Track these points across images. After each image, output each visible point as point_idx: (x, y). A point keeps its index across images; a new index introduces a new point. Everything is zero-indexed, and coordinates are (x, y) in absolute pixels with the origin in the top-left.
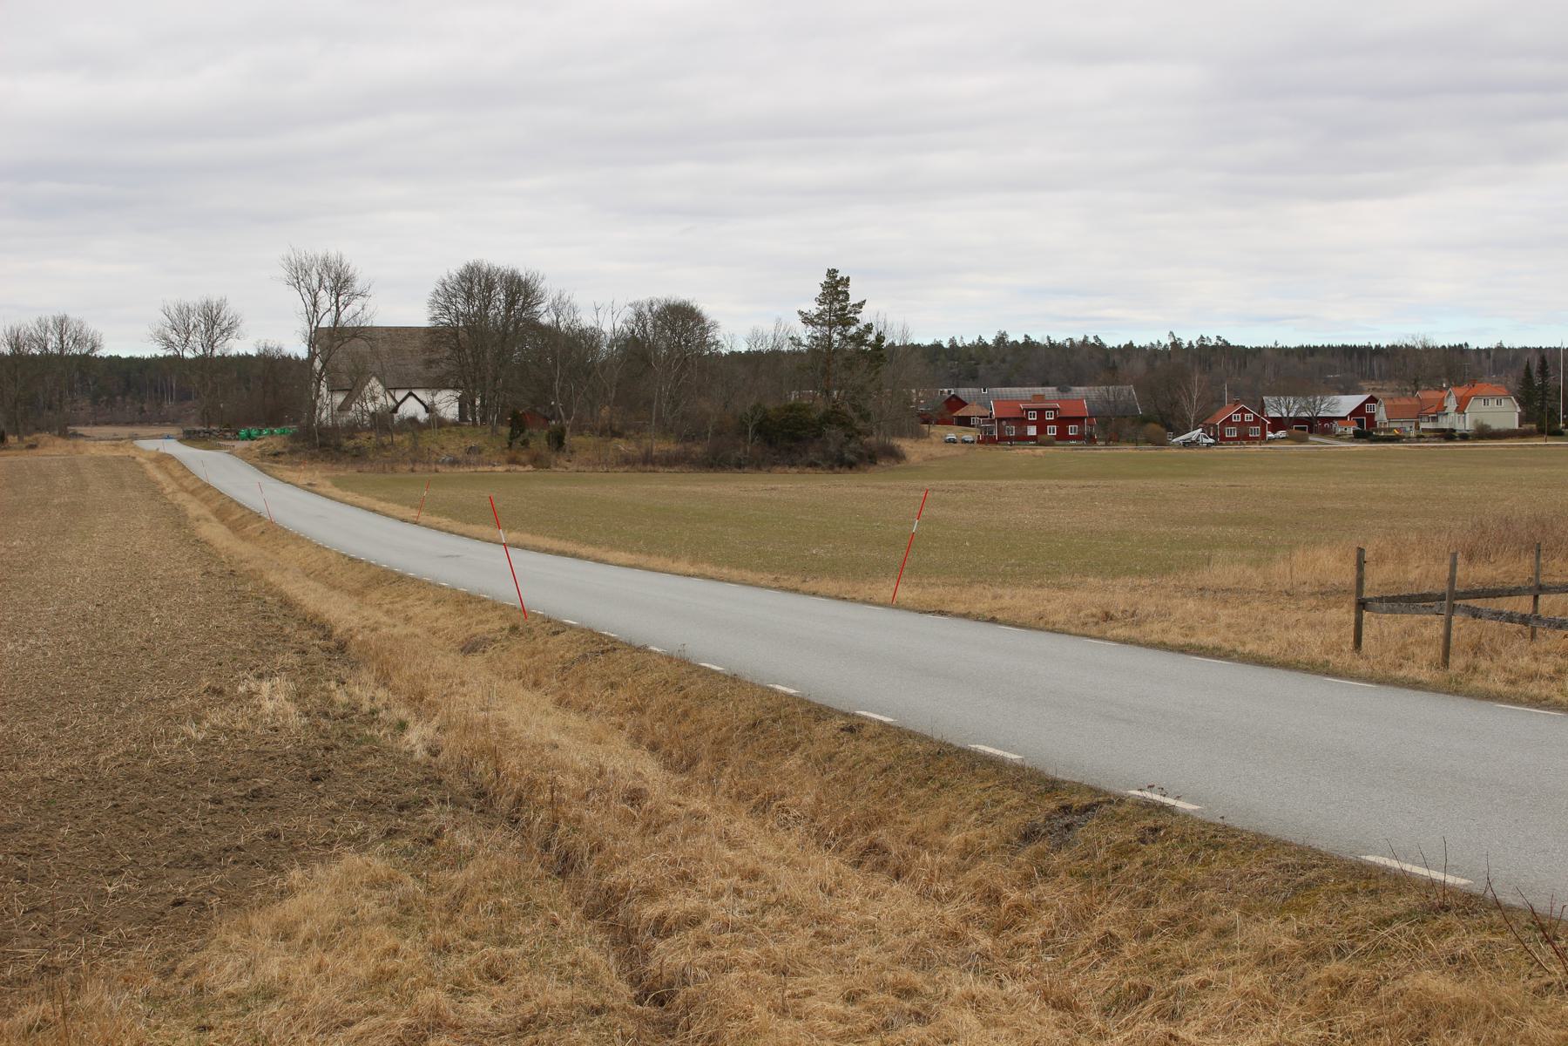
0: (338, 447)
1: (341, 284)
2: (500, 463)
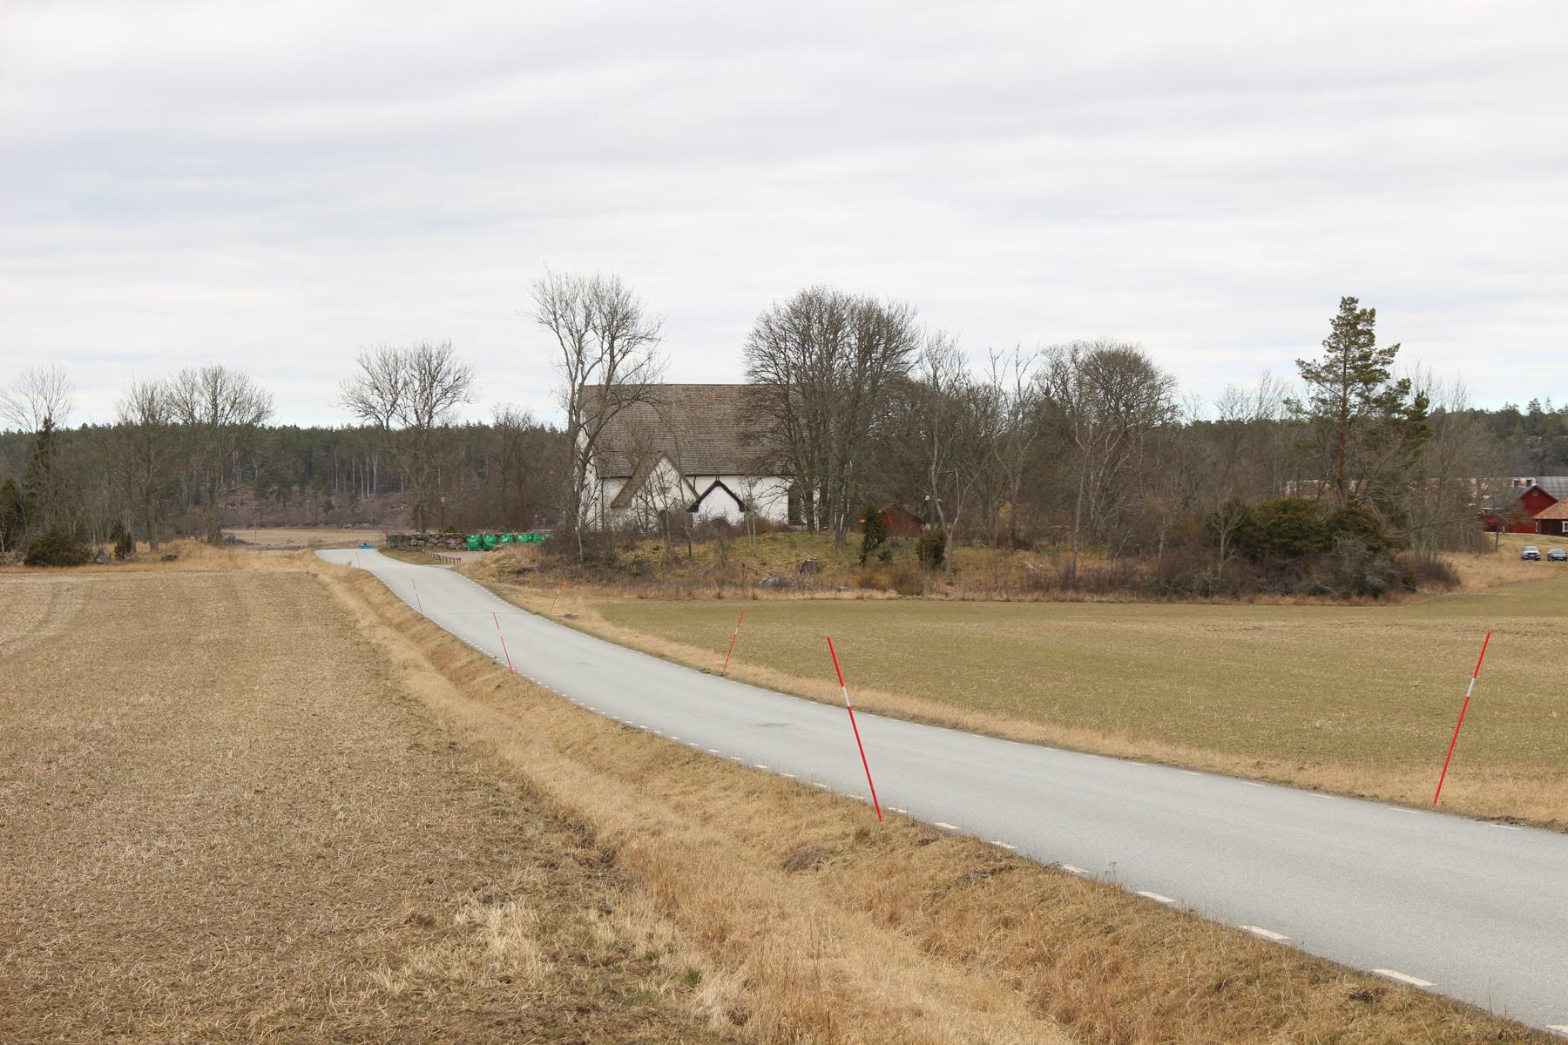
0: (611, 561)
1: (618, 323)
2: (848, 587)
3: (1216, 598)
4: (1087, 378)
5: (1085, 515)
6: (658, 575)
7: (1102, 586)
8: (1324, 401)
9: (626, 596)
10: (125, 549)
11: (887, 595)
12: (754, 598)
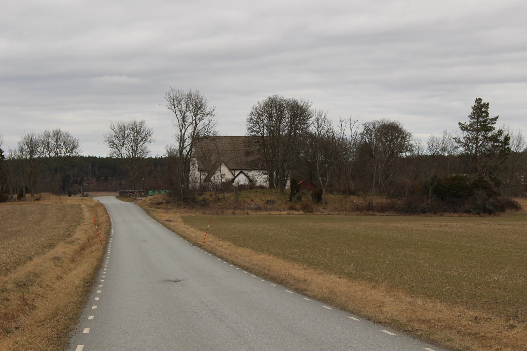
0: (193, 200)
1: (198, 108)
2: (284, 210)
3: (428, 214)
4: (378, 134)
5: (377, 183)
6: (211, 205)
7: (383, 209)
8: (469, 138)
9: (197, 213)
10: (21, 197)
11: (299, 213)
12: (247, 214)
